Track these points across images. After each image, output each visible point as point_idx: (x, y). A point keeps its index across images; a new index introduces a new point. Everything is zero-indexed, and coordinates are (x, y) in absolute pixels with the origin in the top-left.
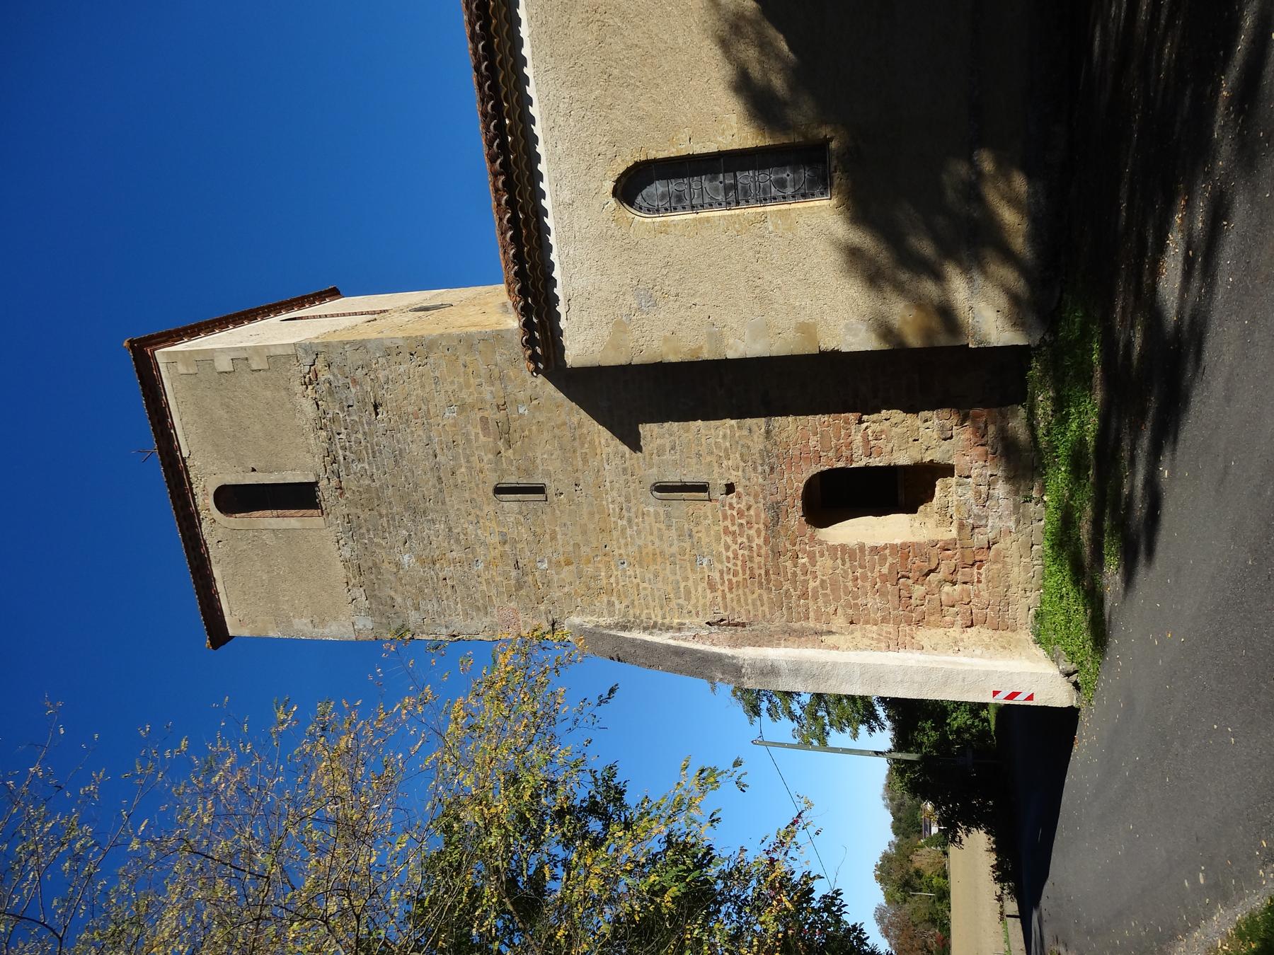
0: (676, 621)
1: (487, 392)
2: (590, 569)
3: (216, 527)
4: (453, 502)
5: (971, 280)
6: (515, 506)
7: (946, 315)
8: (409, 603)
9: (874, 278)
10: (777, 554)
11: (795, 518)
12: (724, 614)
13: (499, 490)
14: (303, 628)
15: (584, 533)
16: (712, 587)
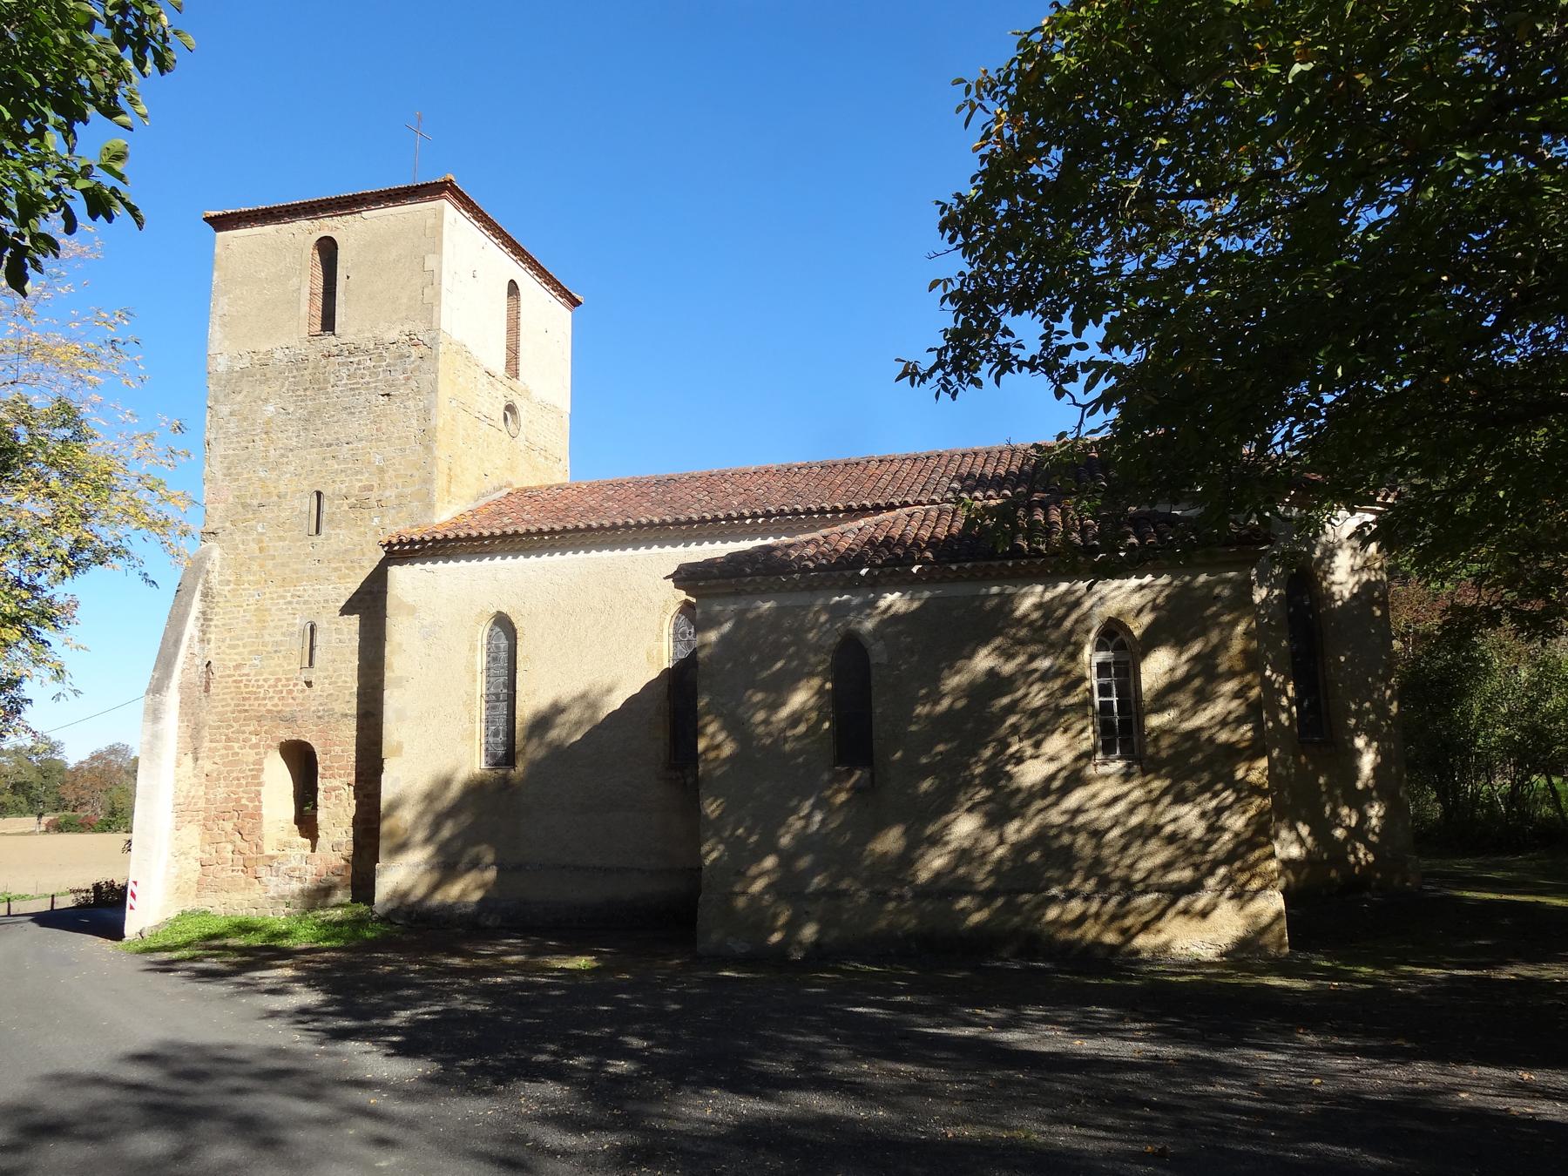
0: (213, 637)
1: (390, 493)
2: (255, 567)
3: (306, 231)
4: (313, 455)
5: (418, 865)
6: (306, 508)
7: (401, 847)
8: (236, 407)
9: (430, 797)
10: (259, 719)
11: (286, 735)
12: (217, 674)
13: (319, 494)
14: (221, 305)
15: (283, 565)
16: (237, 667)
